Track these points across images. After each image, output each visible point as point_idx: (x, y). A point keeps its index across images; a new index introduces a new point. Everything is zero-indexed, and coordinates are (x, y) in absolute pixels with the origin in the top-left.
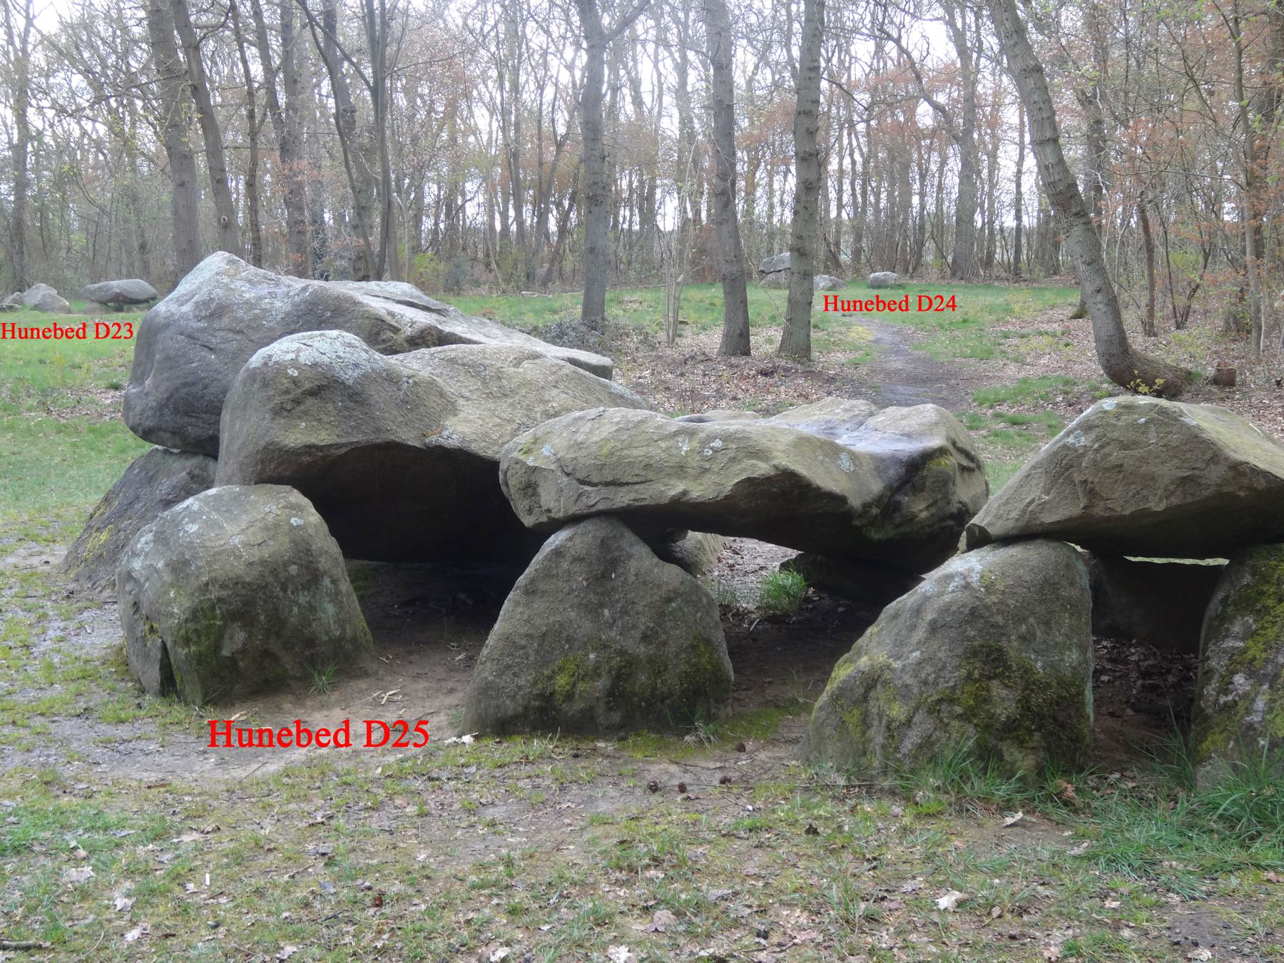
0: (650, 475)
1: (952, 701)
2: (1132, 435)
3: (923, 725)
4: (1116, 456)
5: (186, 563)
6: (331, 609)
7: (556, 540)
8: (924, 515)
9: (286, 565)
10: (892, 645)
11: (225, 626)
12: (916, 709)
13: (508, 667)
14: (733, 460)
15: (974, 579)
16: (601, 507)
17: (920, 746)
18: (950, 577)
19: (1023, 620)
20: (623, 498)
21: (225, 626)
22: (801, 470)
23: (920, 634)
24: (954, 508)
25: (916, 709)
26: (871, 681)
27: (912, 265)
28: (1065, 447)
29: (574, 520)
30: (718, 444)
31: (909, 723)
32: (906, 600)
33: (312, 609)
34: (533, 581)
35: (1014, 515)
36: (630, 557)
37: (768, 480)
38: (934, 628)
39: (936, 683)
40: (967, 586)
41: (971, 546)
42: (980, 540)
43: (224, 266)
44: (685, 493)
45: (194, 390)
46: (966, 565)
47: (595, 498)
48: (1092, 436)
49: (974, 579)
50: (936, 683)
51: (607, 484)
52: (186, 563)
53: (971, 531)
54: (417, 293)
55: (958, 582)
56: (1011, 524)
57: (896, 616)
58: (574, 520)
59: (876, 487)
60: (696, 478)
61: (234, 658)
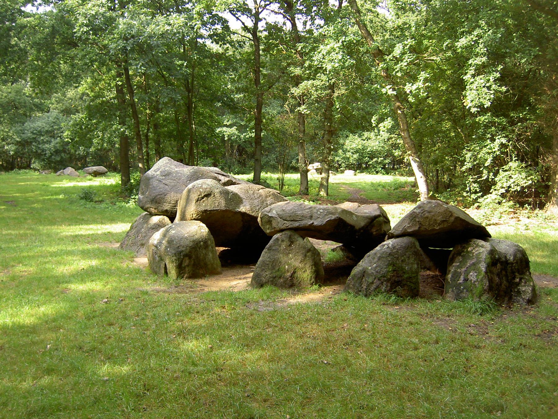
0: (303, 218)
1: (384, 277)
2: (431, 209)
3: (377, 282)
4: (427, 215)
5: (173, 241)
6: (211, 255)
7: (275, 237)
8: (374, 233)
9: (200, 242)
10: (368, 263)
11: (183, 258)
12: (375, 279)
13: (264, 269)
14: (326, 215)
15: (390, 245)
16: (289, 227)
17: (376, 288)
18: (384, 245)
19: (403, 256)
20: (296, 224)
21: (183, 258)
22: (343, 218)
23: (376, 260)
24: (383, 232)
25: (375, 279)
26: (364, 273)
27: (103, 117)
28: (414, 212)
29: (281, 231)
30: (321, 211)
31: (372, 283)
32: (372, 252)
33: (206, 254)
34: (270, 246)
35: (401, 229)
36: (297, 241)
37: (335, 220)
38: (379, 259)
39: (380, 272)
40: (388, 247)
41: (388, 239)
42: (392, 237)
43: (167, 161)
44: (313, 223)
45: (161, 196)
46: (389, 243)
47: (288, 224)
48: (421, 210)
49: (390, 245)
50: (380, 272)
51: (292, 221)
52: (173, 241)
53: (388, 235)
54: (220, 170)
55: (386, 246)
56: (399, 232)
57: (368, 256)
58: (281, 231)
59: (362, 224)
60: (315, 219)
61: (192, 263)
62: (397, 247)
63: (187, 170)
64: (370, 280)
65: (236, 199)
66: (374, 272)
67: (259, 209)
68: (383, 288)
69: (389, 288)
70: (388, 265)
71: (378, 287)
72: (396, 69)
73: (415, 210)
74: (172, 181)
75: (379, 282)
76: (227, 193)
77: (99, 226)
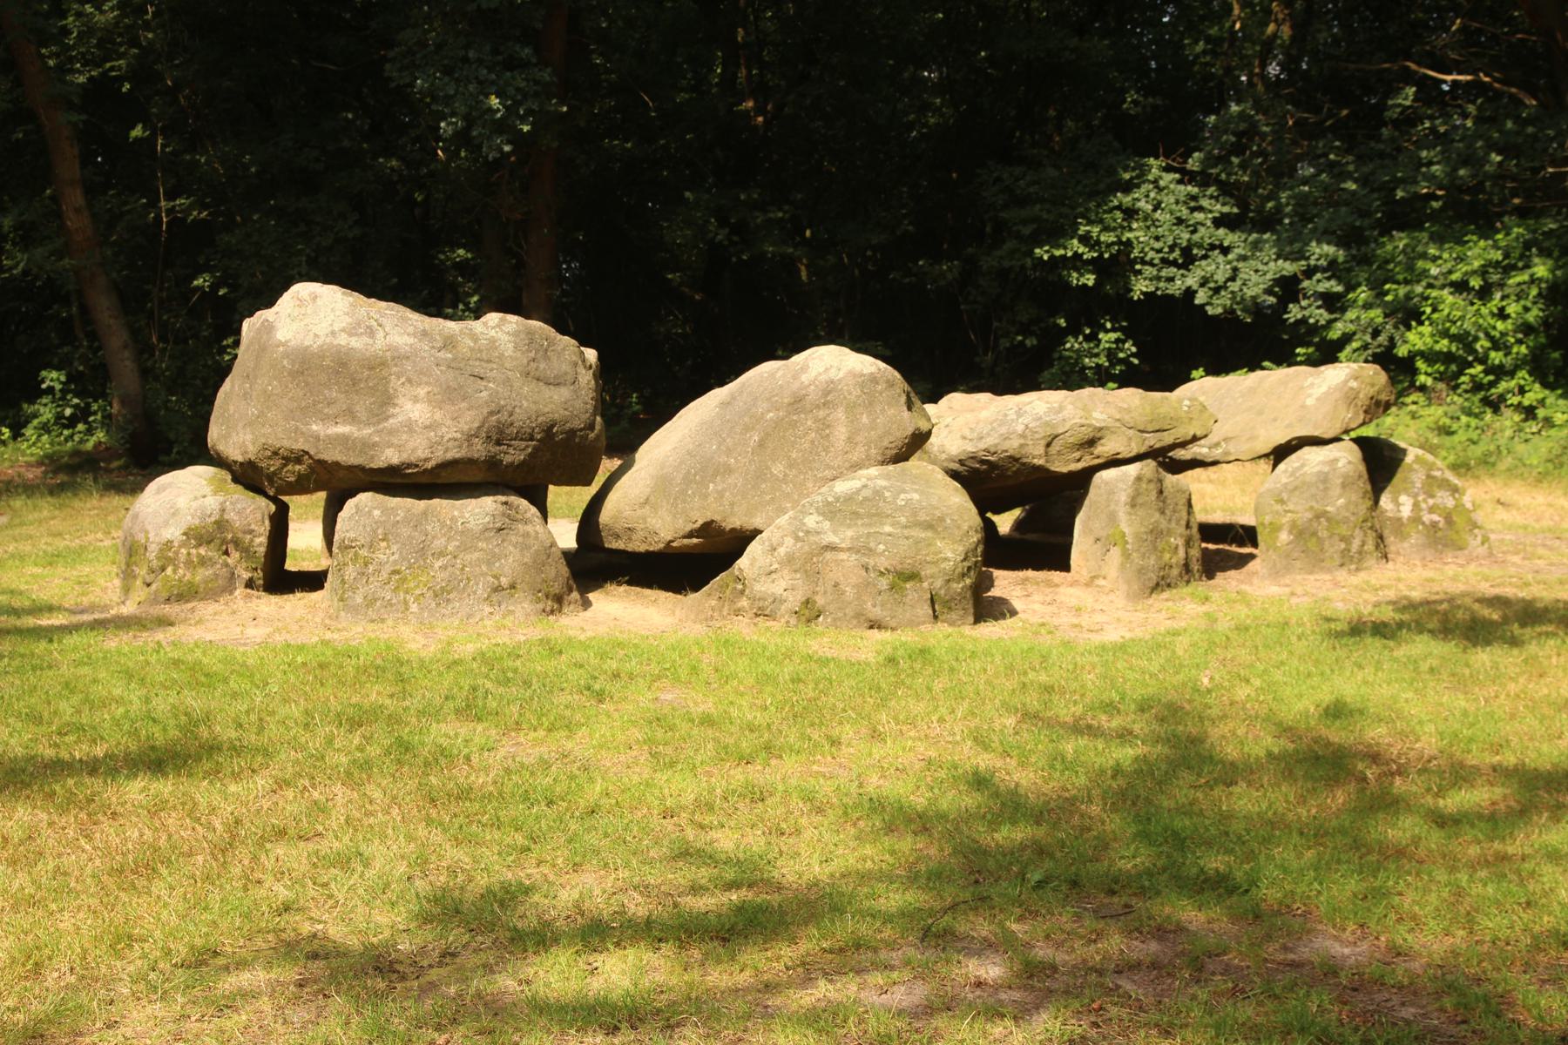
30: (1187, 402)
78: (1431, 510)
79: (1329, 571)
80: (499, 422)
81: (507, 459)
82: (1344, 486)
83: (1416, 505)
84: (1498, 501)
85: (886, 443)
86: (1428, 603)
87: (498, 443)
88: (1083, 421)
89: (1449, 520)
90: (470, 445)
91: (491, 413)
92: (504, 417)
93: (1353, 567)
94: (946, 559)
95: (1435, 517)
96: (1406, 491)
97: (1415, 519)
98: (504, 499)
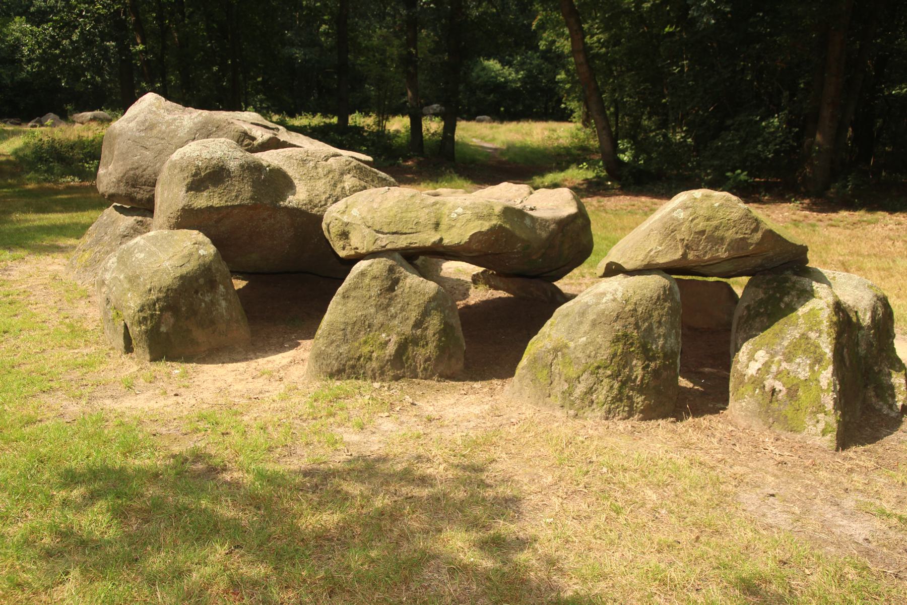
11: (160, 315)
16: (388, 247)
20: (402, 242)
23: (586, 327)
28: (673, 219)
30: (460, 210)
44: (441, 240)
47: (385, 241)
52: (138, 277)
59: (572, 166)
62: (634, 300)
63: (192, 117)
64: (572, 372)
65: (279, 182)
66: (580, 355)
67: (326, 200)
68: (602, 394)
69: (615, 392)
70: (616, 340)
71: (590, 391)
72: (636, 377)
73: (675, 214)
74: (158, 141)
75: (592, 380)
76: (257, 168)
77: (60, 216)
78: (778, 376)
79: (551, 406)
80: (135, 174)
81: (139, 196)
82: (594, 324)
83: (767, 365)
84: (223, 434)
85: (168, 214)
86: (235, 519)
87: (133, 186)
88: (339, 216)
89: (792, 393)
90: (119, 186)
91: (131, 169)
92: (139, 172)
93: (572, 412)
94: (130, 307)
95: (778, 386)
96: (768, 346)
97: (757, 382)
98: (140, 218)
